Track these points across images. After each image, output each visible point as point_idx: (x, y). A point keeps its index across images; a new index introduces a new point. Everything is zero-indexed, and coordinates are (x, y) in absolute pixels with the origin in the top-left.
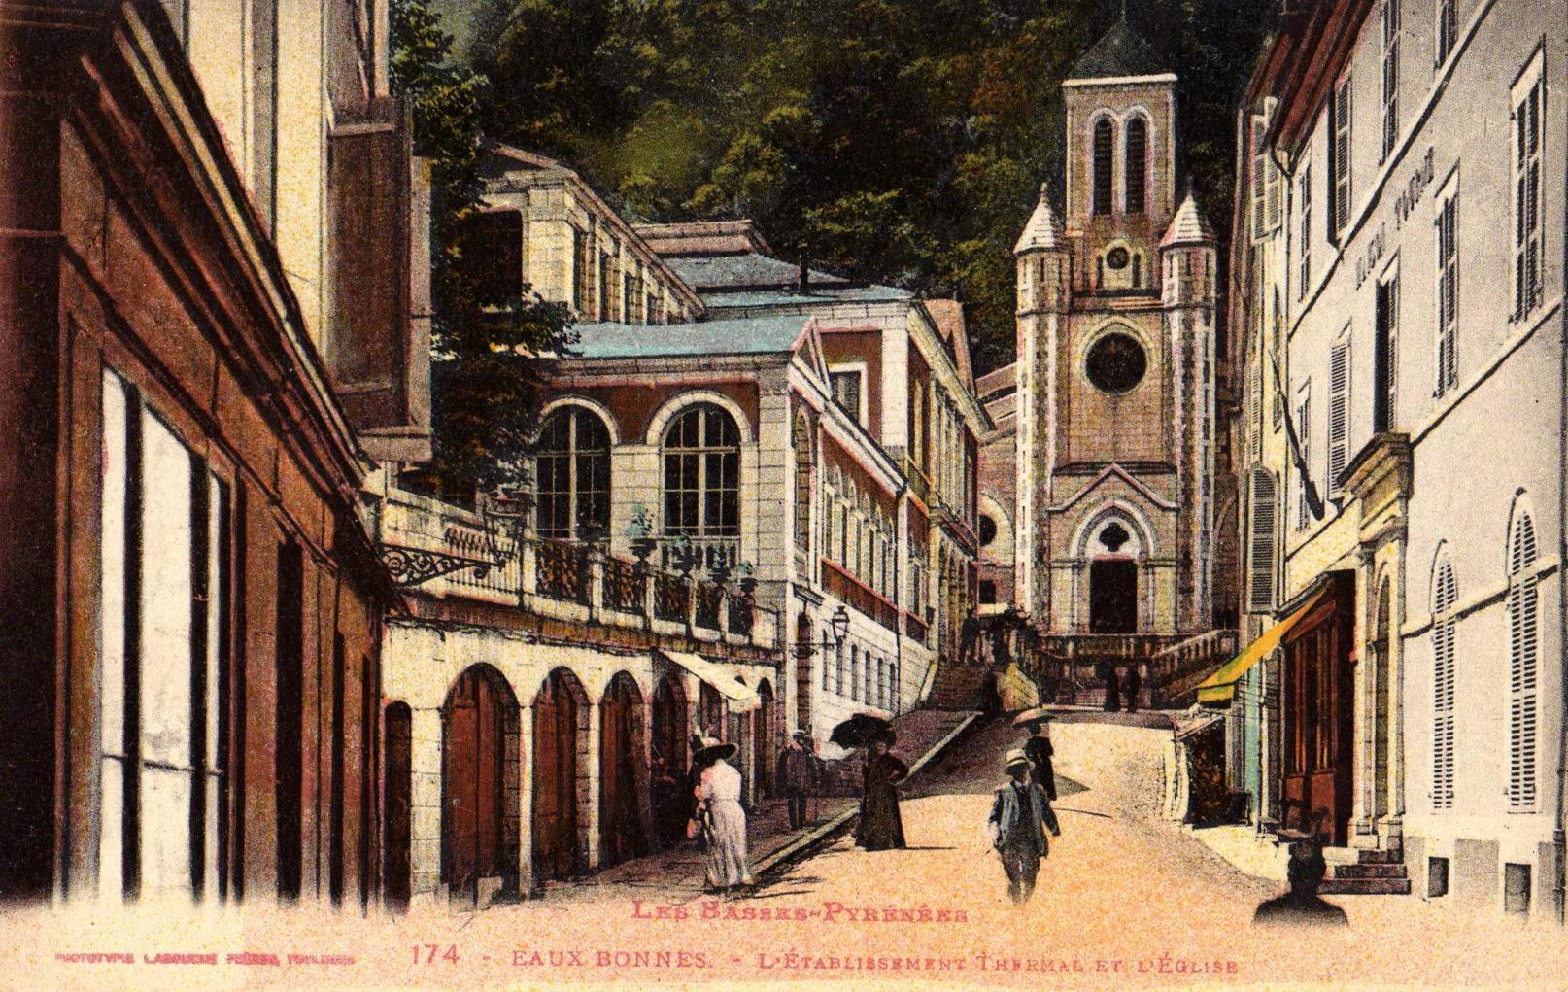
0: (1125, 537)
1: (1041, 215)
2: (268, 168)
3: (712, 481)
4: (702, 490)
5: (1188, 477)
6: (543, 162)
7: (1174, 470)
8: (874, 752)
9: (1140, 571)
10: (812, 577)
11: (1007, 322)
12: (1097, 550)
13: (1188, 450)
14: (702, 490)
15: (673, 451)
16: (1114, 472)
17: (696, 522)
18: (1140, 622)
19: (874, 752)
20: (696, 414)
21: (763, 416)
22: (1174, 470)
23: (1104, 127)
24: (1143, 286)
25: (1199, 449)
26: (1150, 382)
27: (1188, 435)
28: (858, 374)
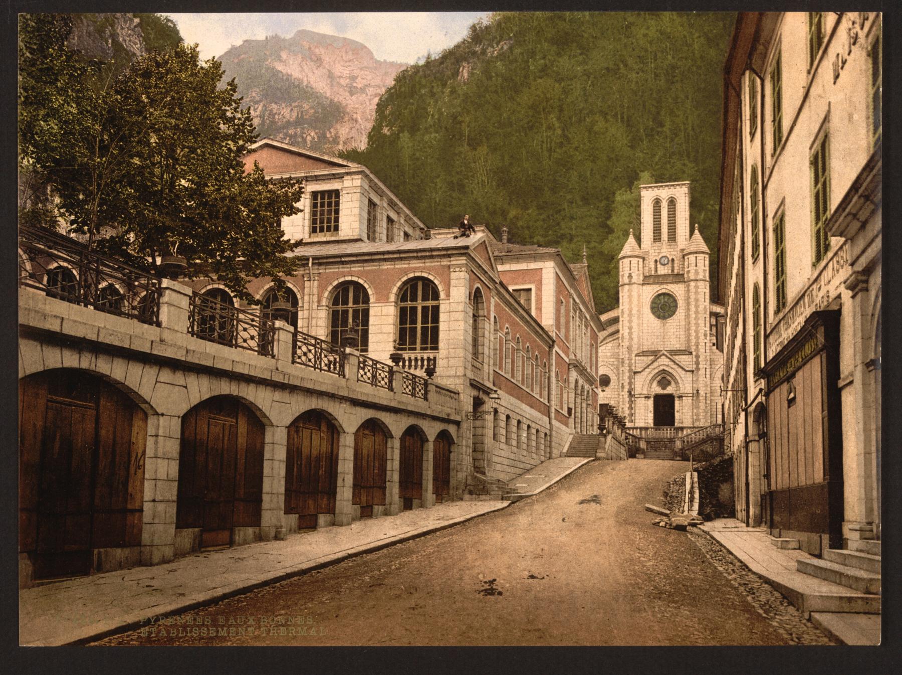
0: (669, 383)
1: (631, 240)
2: (448, 393)
3: (425, 320)
4: (419, 326)
5: (697, 357)
6: (349, 164)
7: (691, 353)
8: (255, 251)
9: (676, 399)
10: (486, 378)
11: (608, 273)
12: (657, 390)
13: (697, 345)
14: (419, 326)
15: (403, 304)
16: (663, 354)
17: (415, 343)
18: (676, 421)
19: (255, 251)
20: (416, 284)
21: (452, 282)
22: (691, 353)
23: (657, 203)
24: (676, 272)
25: (702, 344)
26: (680, 312)
27: (697, 337)
28: (530, 290)
